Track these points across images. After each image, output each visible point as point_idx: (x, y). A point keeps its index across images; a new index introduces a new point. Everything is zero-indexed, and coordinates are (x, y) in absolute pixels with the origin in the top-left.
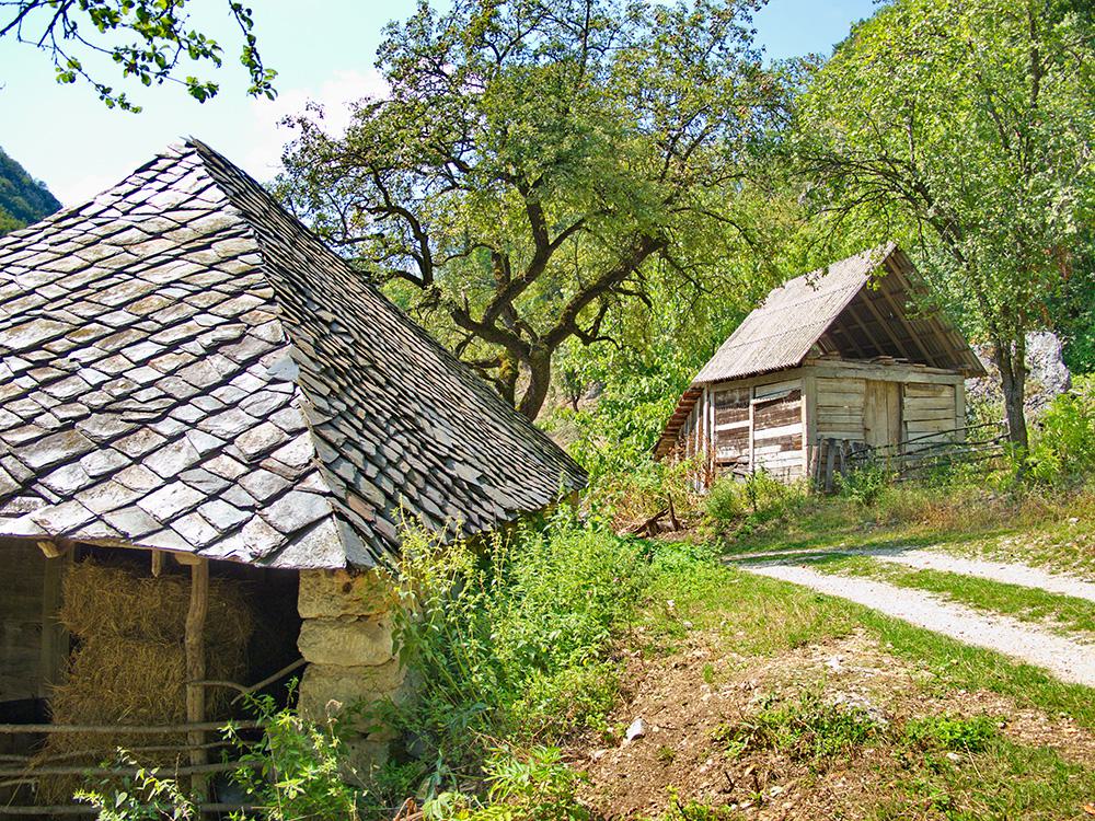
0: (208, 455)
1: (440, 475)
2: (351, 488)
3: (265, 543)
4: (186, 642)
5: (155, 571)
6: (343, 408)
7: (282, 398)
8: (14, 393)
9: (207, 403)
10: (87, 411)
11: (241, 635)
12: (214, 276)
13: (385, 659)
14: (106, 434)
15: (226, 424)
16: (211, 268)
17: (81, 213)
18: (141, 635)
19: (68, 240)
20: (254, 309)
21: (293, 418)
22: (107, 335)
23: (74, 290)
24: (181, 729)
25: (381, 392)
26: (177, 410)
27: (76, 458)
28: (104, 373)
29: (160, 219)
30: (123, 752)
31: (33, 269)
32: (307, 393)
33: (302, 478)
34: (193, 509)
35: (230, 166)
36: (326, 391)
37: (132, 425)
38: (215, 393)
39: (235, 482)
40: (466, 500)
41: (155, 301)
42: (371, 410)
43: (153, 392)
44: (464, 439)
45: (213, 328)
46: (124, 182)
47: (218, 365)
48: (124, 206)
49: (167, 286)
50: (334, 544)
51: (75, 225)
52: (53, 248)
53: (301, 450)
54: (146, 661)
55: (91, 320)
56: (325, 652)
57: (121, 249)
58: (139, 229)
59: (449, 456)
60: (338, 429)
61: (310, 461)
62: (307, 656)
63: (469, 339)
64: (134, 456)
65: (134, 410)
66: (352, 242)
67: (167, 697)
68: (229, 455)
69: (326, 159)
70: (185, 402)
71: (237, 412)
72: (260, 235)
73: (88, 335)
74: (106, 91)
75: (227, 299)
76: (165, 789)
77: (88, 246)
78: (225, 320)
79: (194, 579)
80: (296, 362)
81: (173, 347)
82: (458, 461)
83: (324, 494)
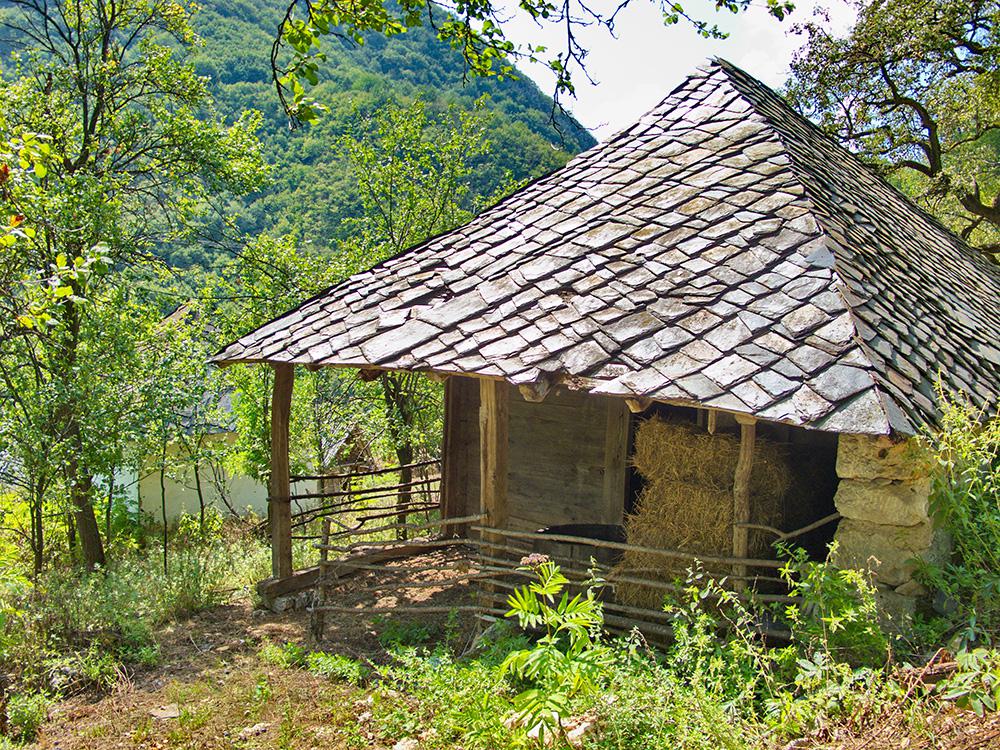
0: (759, 332)
1: (967, 355)
2: (889, 363)
3: (814, 409)
4: (735, 490)
5: (711, 429)
6: (876, 292)
7: (820, 283)
8: (598, 283)
9: (754, 288)
10: (655, 296)
11: (780, 488)
12: (748, 178)
13: (917, 521)
14: (672, 314)
15: (773, 306)
16: (744, 170)
17: (631, 133)
18: (696, 481)
19: (623, 157)
20: (788, 204)
21: (831, 300)
22: (664, 233)
23: (633, 198)
24: (728, 561)
25: (905, 277)
26: (728, 294)
27: (650, 334)
28: (665, 264)
29: (695, 132)
30: (698, 562)
31: (599, 182)
32: (844, 278)
33: (845, 353)
34: (749, 378)
35: (749, 78)
36: (859, 276)
37: (693, 307)
38: (759, 280)
39: (784, 355)
40: (994, 380)
41: (699, 203)
42: (899, 293)
43: (707, 280)
44: (985, 322)
45: (753, 223)
46: (662, 103)
47: (760, 256)
48: (664, 124)
49: (708, 189)
50: (877, 412)
51: (626, 144)
52: (612, 165)
53: (842, 328)
54: (700, 502)
55: (649, 221)
56: (860, 509)
57: (666, 160)
58: (679, 142)
59: (973, 338)
60: (874, 311)
61: (852, 338)
62: (842, 511)
63: (975, 224)
64: (696, 333)
65: (694, 295)
66: (857, 137)
67: (717, 533)
68: (777, 332)
69: (833, 59)
70: (734, 287)
71: (780, 295)
72: (784, 138)
73: (649, 234)
74: (702, 26)
75: (762, 198)
76: (730, 600)
77: (639, 160)
78: (762, 216)
79: (743, 438)
80: (831, 251)
81: (719, 241)
82: (984, 344)
83: (866, 369)
